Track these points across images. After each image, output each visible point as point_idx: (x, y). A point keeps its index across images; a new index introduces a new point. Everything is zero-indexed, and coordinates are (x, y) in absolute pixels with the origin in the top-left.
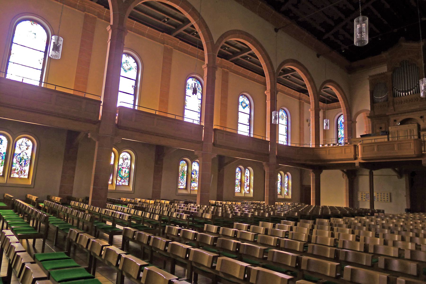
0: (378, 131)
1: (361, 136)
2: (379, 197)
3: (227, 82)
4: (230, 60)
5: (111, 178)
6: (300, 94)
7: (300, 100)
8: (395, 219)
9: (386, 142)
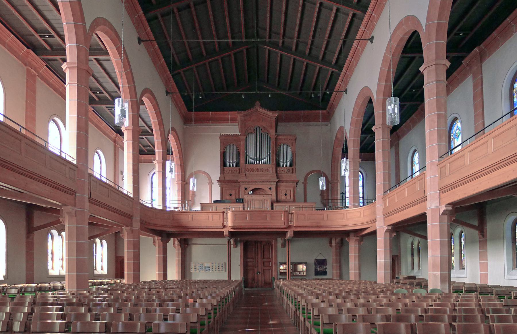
0: (228, 197)
1: (214, 201)
2: (214, 267)
3: (35, 92)
4: (43, 57)
5: (94, 246)
6: (116, 136)
7: (115, 142)
8: (138, 290)
9: (241, 211)
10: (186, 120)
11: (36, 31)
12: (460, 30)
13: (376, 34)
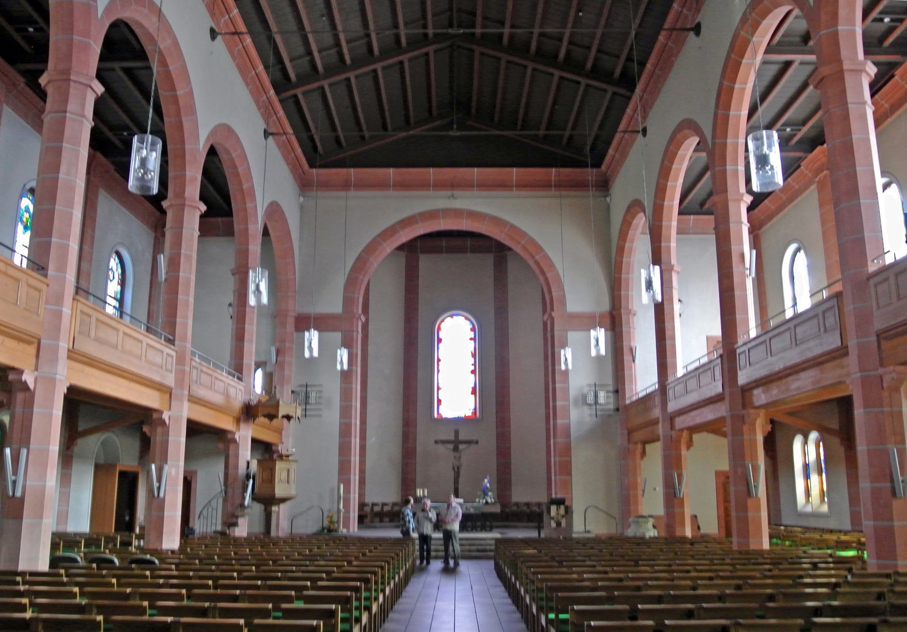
4: (23, 67)
10: (304, 185)
11: (111, 129)
12: (884, 12)
13: (651, 124)
